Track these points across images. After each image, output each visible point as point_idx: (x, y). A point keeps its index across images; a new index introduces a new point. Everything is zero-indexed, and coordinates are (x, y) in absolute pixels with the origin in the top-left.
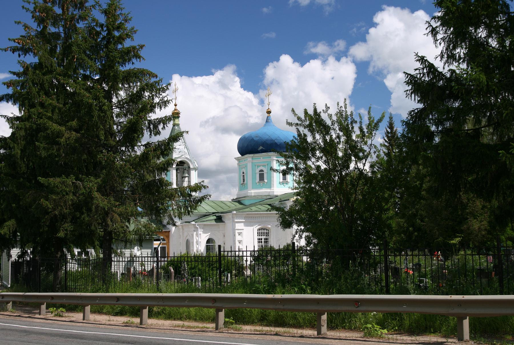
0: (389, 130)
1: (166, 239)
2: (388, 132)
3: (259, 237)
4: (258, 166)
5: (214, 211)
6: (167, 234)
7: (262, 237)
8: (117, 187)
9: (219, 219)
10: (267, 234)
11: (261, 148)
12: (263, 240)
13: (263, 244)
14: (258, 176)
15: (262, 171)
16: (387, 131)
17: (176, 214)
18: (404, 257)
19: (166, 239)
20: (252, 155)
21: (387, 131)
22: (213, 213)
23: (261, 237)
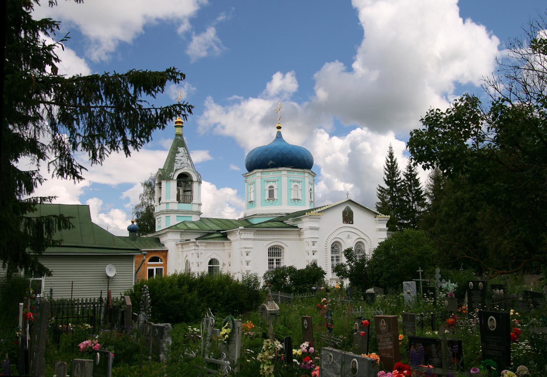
0: (389, 160)
1: (163, 259)
2: (388, 162)
3: (270, 258)
4: (268, 182)
5: (220, 229)
6: (164, 254)
7: (274, 257)
8: (34, 148)
9: (225, 236)
10: (279, 254)
11: (271, 162)
12: (275, 261)
13: (275, 266)
14: (267, 193)
15: (271, 187)
16: (387, 160)
17: (79, 140)
18: (85, 316)
19: (163, 259)
20: (261, 170)
21: (387, 160)
22: (218, 231)
23: (272, 258)
